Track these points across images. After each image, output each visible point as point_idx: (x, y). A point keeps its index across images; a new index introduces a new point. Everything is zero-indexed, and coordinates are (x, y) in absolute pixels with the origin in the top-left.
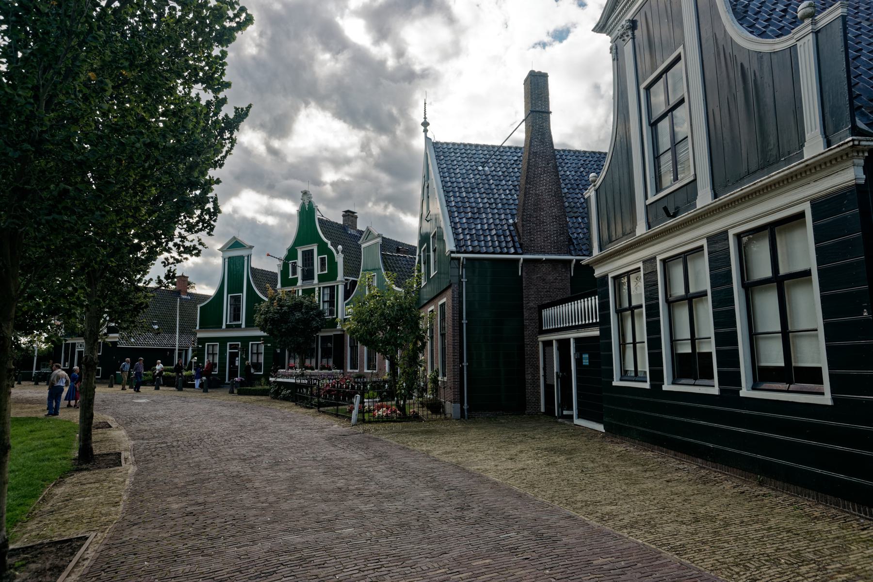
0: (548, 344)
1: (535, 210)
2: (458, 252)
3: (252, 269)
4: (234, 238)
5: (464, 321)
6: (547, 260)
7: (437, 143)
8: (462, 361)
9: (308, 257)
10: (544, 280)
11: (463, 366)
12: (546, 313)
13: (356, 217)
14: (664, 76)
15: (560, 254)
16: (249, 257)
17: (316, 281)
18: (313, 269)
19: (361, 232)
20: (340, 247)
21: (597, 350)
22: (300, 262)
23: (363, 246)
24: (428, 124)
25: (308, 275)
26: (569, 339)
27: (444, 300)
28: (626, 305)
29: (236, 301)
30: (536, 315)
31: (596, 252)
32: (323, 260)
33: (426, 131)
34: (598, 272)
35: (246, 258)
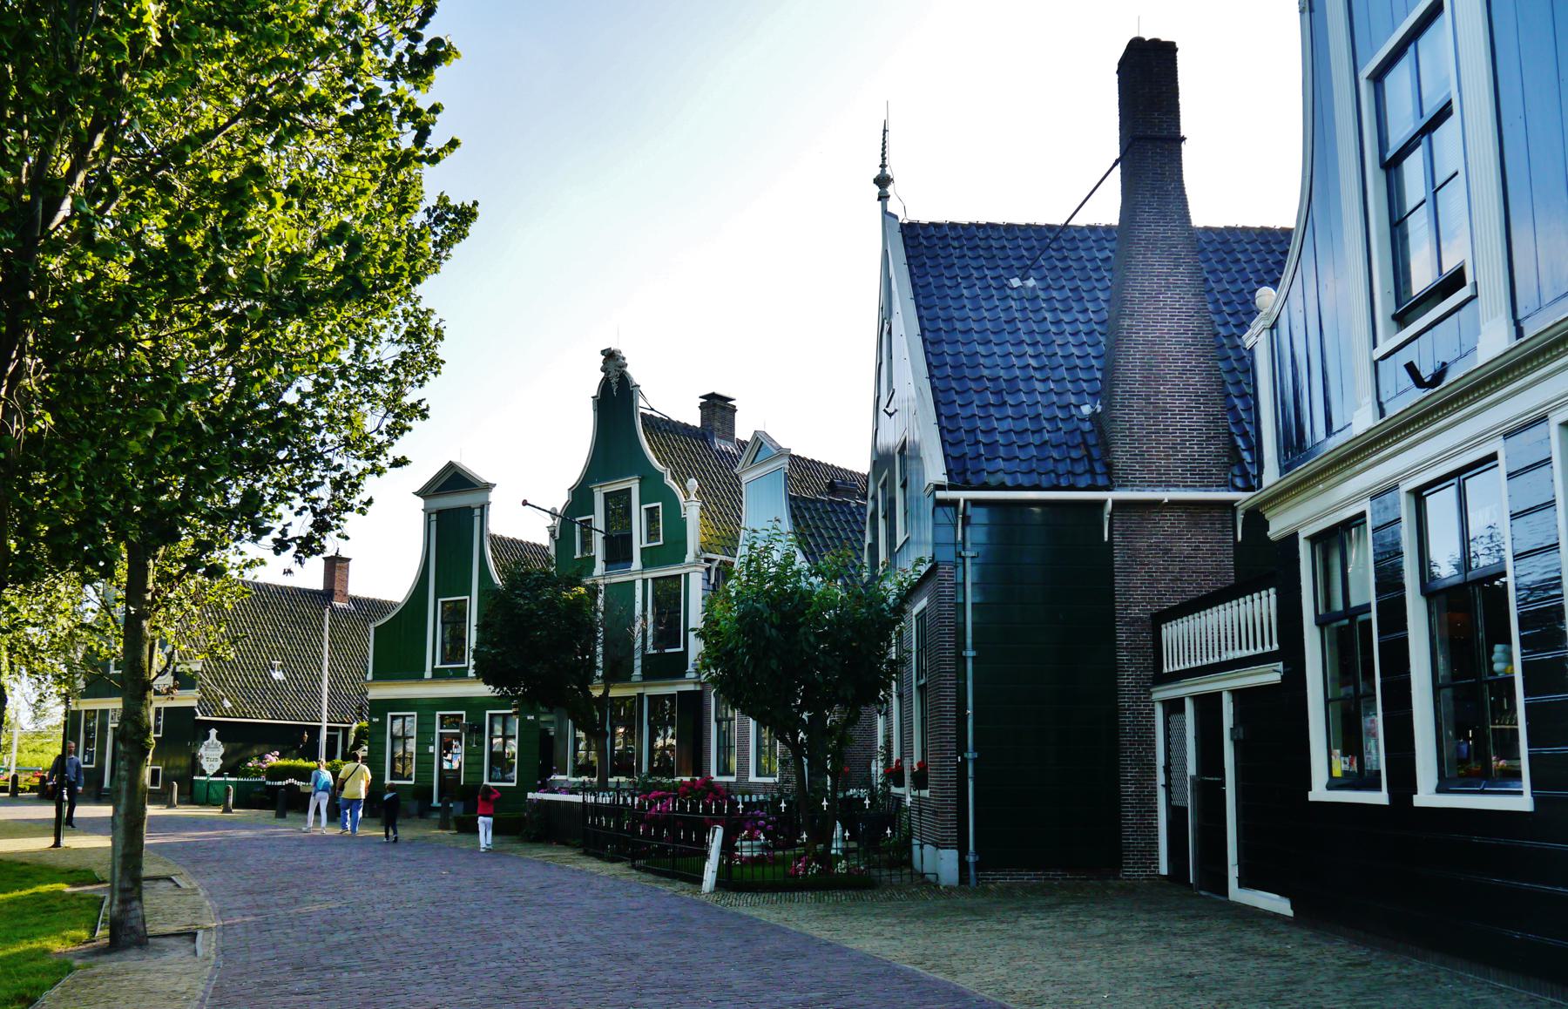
0: (1174, 707)
1: (1146, 381)
2: (952, 488)
3: (493, 538)
4: (451, 465)
5: (970, 653)
6: (1174, 504)
7: (912, 225)
8: (961, 748)
9: (618, 506)
10: (1167, 551)
11: (965, 760)
12: (1172, 632)
13: (733, 409)
14: (1411, 49)
15: (1207, 487)
16: (484, 508)
17: (637, 563)
18: (630, 536)
19: (743, 445)
20: (693, 484)
21: (1273, 719)
22: (599, 520)
23: (745, 478)
24: (878, 181)
25: (618, 551)
26: (1218, 696)
27: (924, 603)
28: (1338, 605)
29: (454, 617)
30: (1145, 637)
31: (1271, 474)
32: (652, 513)
33: (883, 197)
34: (1277, 527)
35: (477, 512)
